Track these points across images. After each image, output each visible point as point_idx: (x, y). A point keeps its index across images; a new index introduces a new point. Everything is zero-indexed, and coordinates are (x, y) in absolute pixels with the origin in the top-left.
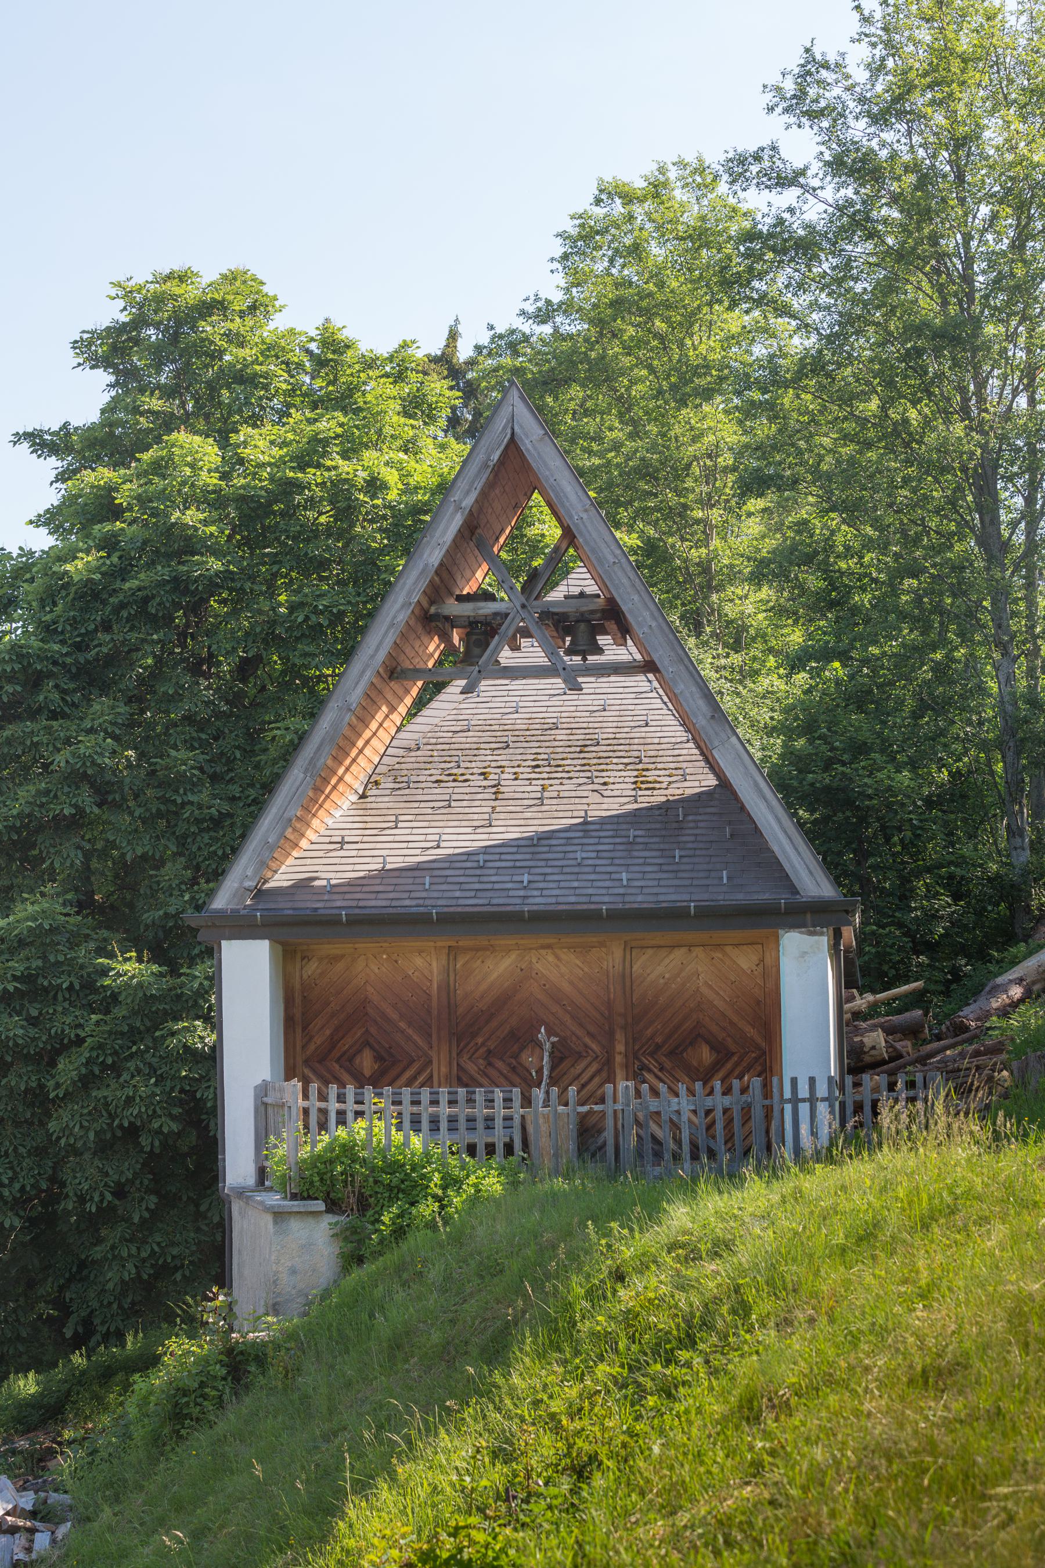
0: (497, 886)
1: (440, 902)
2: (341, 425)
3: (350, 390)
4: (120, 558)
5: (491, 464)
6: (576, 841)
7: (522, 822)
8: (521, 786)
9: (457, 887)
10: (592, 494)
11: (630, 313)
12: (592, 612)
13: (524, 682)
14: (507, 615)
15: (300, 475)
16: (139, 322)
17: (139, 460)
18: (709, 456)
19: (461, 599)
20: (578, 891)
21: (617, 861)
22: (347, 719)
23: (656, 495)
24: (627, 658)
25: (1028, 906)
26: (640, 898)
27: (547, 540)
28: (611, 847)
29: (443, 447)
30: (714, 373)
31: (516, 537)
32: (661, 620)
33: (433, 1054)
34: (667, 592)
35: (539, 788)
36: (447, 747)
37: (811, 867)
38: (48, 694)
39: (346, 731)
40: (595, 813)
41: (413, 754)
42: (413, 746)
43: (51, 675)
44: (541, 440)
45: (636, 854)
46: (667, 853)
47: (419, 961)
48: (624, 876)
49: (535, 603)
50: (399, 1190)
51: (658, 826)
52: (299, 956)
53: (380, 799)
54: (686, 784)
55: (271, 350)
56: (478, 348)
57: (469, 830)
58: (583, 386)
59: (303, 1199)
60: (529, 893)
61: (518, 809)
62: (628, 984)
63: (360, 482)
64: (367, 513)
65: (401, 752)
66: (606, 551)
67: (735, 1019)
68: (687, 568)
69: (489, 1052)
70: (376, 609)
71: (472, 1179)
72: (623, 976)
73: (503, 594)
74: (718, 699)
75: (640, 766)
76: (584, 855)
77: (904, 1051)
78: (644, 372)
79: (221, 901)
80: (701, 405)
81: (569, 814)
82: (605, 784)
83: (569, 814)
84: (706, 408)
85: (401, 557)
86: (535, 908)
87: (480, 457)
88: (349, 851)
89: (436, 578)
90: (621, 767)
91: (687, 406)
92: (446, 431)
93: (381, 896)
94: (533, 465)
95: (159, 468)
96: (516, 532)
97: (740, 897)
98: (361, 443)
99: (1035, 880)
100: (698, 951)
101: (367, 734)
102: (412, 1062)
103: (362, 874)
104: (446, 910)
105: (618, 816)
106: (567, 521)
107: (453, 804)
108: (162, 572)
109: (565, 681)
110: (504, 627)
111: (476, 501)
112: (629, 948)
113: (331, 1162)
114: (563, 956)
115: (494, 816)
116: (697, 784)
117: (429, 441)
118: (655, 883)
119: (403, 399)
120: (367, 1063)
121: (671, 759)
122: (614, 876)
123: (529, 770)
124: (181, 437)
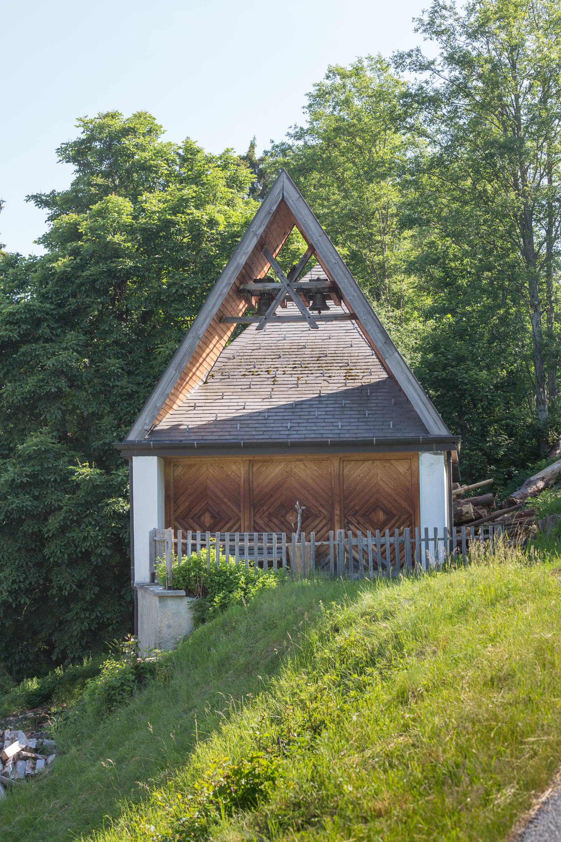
0: (274, 429)
1: (245, 437)
2: (195, 192)
3: (200, 174)
4: (81, 260)
5: (272, 212)
6: (315, 406)
7: (287, 396)
8: (287, 378)
9: (254, 429)
10: (324, 228)
11: (344, 135)
12: (324, 288)
13: (288, 324)
14: (280, 290)
15: (173, 217)
16: (91, 139)
17: (91, 209)
18: (384, 208)
19: (256, 281)
20: (316, 432)
21: (336, 417)
22: (197, 343)
23: (357, 228)
24: (341, 312)
25: (547, 440)
26: (347, 435)
27: (301, 251)
28: (333, 409)
29: (247, 203)
30: (387, 165)
31: (285, 249)
32: (359, 292)
33: (241, 515)
34: (362, 278)
35: (296, 379)
36: (248, 357)
37: (436, 419)
38: (44, 330)
39: (197, 349)
40: (325, 392)
41: (231, 361)
42: (231, 357)
43: (45, 320)
44: (298, 200)
45: (346, 413)
46: (362, 412)
47: (234, 468)
48: (340, 424)
49: (294, 283)
50: (224, 585)
51: (357, 398)
52: (172, 465)
53: (215, 385)
54: (372, 377)
55: (159, 153)
56: (266, 152)
57: (260, 400)
58: (320, 172)
59: (174, 589)
60: (291, 433)
61: (285, 389)
62: (341, 479)
63: (204, 222)
64: (208, 237)
65: (225, 360)
66: (331, 257)
67: (396, 498)
68: (372, 266)
69: (270, 514)
70: (213, 286)
71: (261, 579)
72: (339, 475)
73: (278, 279)
74: (388, 333)
75: (348, 368)
76: (319, 413)
77: (483, 515)
78: (351, 165)
79: (133, 436)
80: (380, 182)
81: (311, 392)
82: (330, 377)
83: (311, 392)
84: (383, 183)
85: (225, 260)
86: (294, 440)
87: (267, 208)
88: (198, 411)
89: (244, 271)
90: (338, 368)
91: (373, 182)
92: (249, 195)
93: (214, 434)
94: (294, 212)
95: (101, 213)
96: (285, 247)
97: (399, 435)
98: (205, 201)
99: (551, 427)
100: (377, 463)
101: (208, 351)
102: (230, 519)
103: (205, 423)
104: (248, 441)
105: (336, 393)
106: (311, 241)
107: (252, 387)
108: (102, 267)
109: (309, 324)
110: (278, 296)
111: (264, 231)
112: (342, 461)
113: (189, 570)
114: (308, 465)
115: (273, 393)
116: (377, 377)
117: (240, 200)
118: (356, 428)
119: (227, 179)
120: (207, 519)
121: (364, 364)
122: (334, 424)
123: (291, 369)
124: (113, 197)
